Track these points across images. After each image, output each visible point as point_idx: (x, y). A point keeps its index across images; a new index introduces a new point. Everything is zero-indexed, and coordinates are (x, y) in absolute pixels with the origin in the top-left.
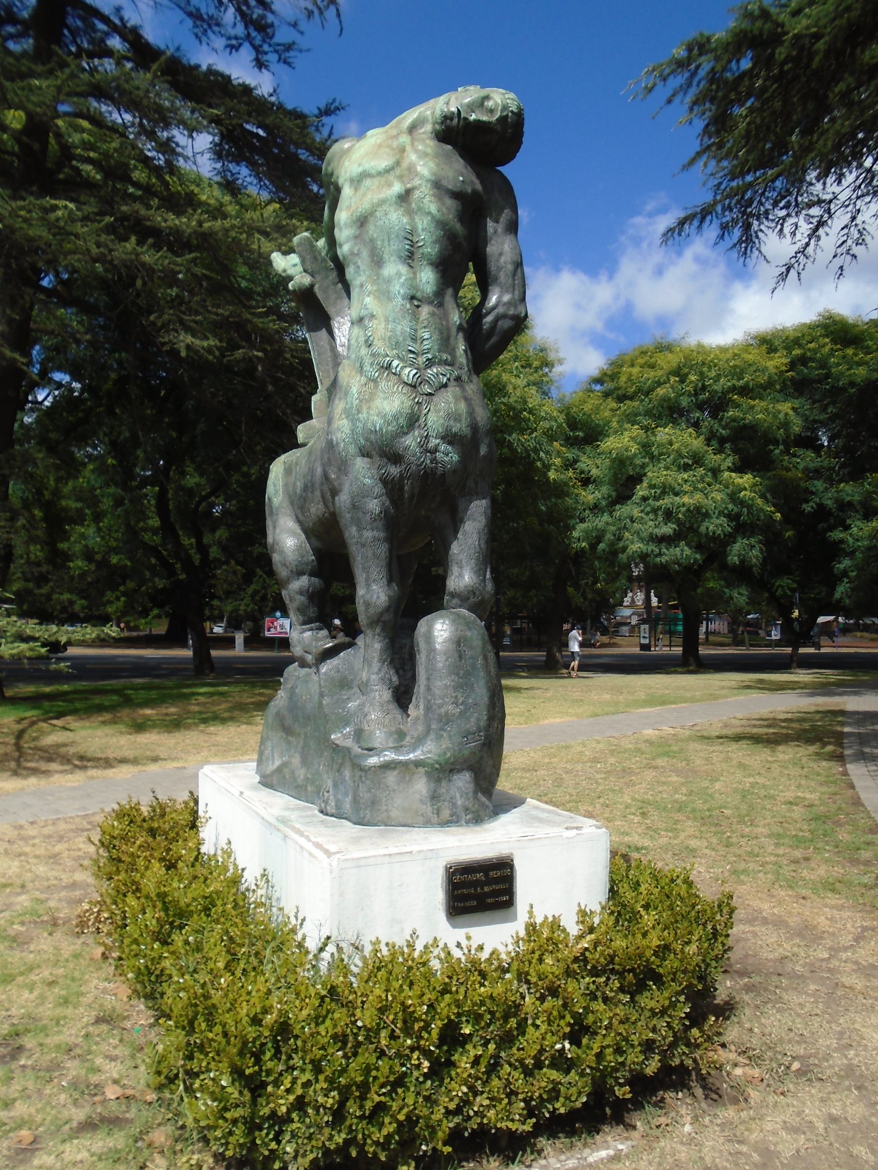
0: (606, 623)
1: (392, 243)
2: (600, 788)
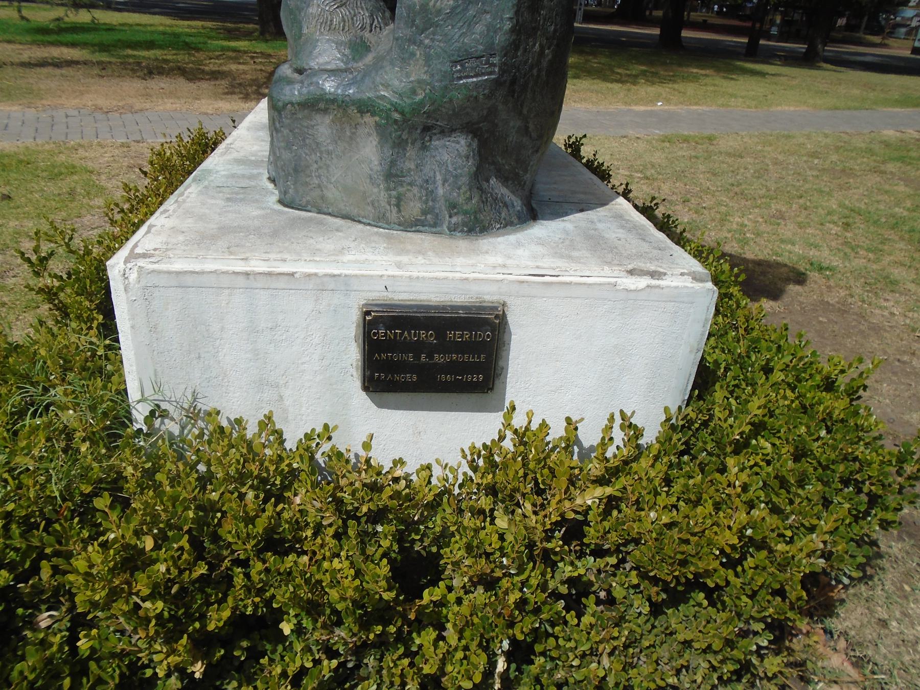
0: (883, 23)
2: (807, 186)
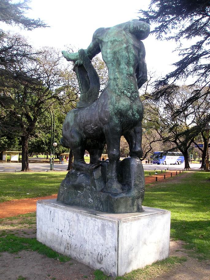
1: (123, 60)
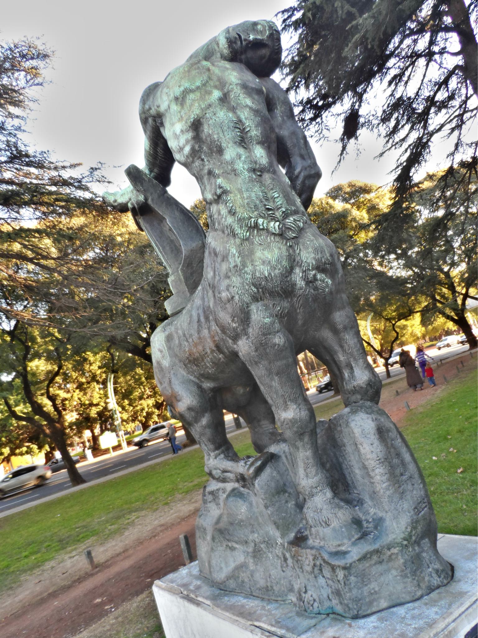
1: (226, 133)
